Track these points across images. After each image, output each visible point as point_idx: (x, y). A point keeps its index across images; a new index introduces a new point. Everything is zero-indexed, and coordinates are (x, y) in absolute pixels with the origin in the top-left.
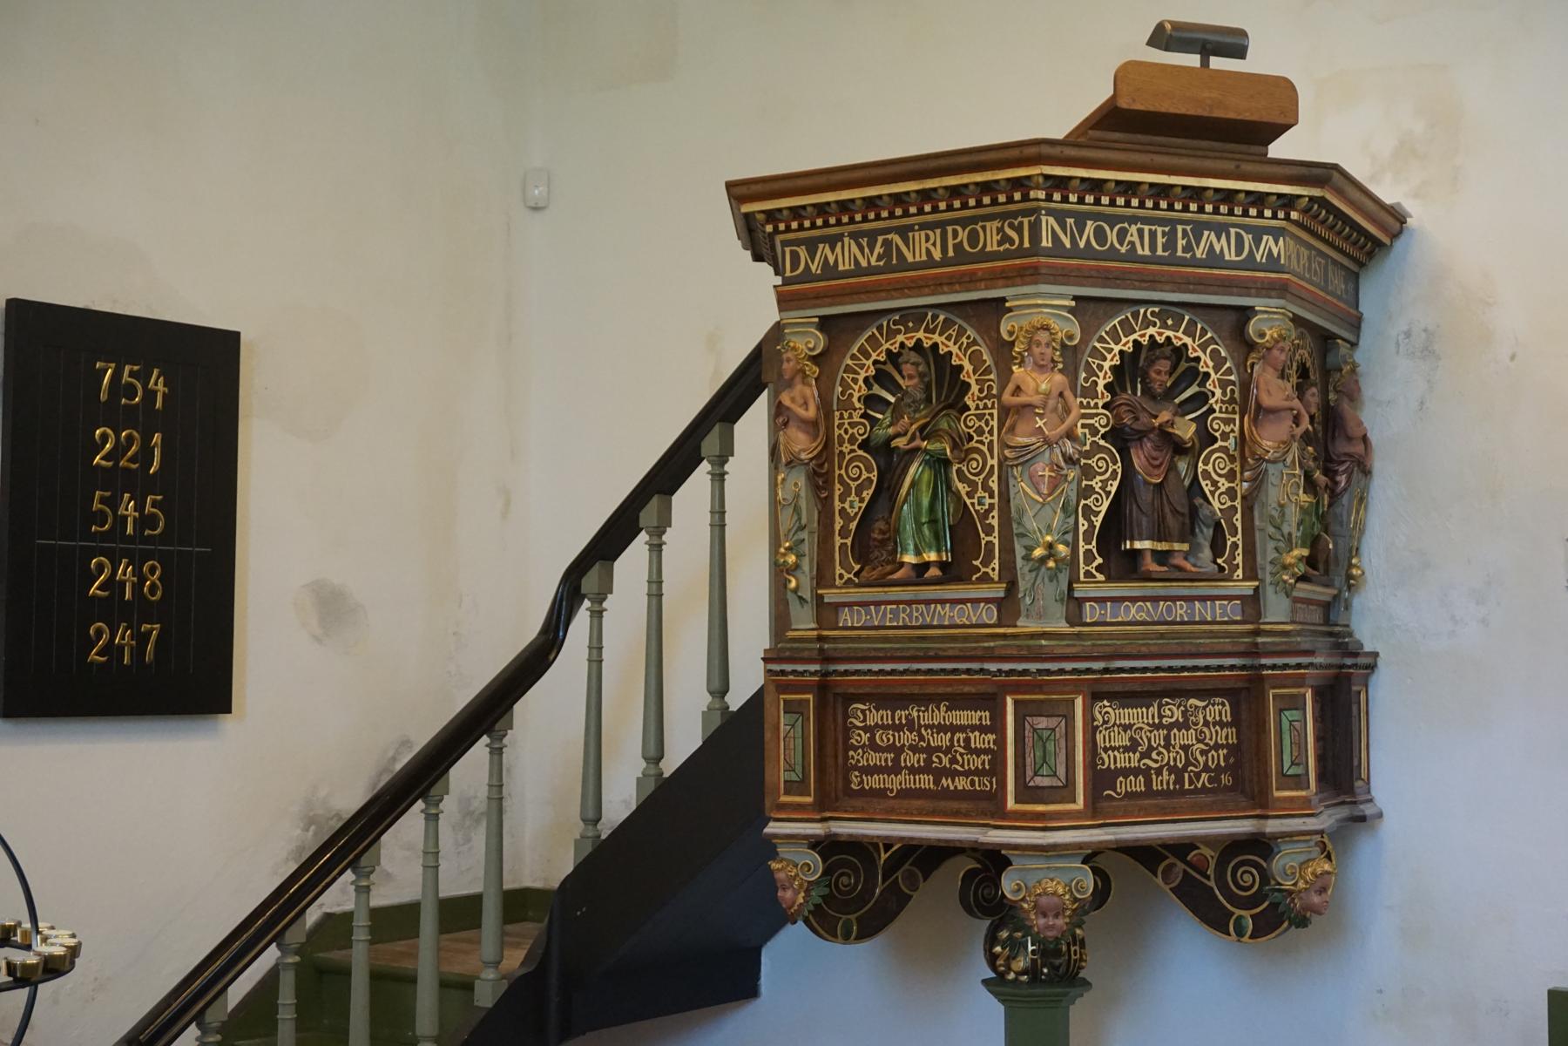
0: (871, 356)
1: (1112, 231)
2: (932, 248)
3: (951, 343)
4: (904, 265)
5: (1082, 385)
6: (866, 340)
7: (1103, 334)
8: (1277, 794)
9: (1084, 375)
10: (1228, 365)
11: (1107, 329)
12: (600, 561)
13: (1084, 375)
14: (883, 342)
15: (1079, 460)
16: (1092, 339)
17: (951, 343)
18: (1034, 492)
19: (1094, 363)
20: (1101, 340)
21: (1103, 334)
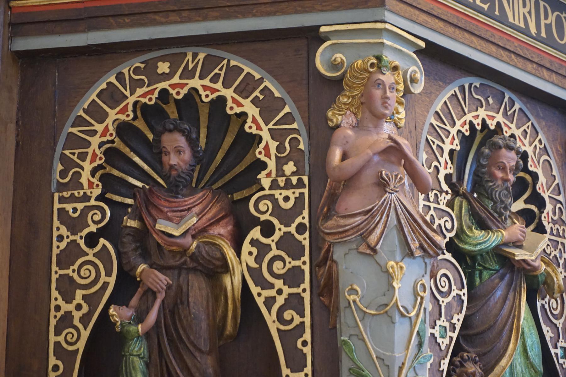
0: (106, 115)
1: (552, 14)
2: (527, 15)
3: (219, 85)
4: (504, 19)
5: (58, 181)
6: (98, 96)
7: (81, 113)
8: (477, 267)
9: (60, 167)
10: (287, 109)
11: (86, 106)
12: (148, 266)
13: (60, 167)
14: (127, 93)
15: (283, 175)
16: (64, 125)
17: (219, 85)
18: (462, 98)
19: (74, 154)
20: (79, 122)
21: (81, 113)
